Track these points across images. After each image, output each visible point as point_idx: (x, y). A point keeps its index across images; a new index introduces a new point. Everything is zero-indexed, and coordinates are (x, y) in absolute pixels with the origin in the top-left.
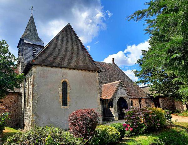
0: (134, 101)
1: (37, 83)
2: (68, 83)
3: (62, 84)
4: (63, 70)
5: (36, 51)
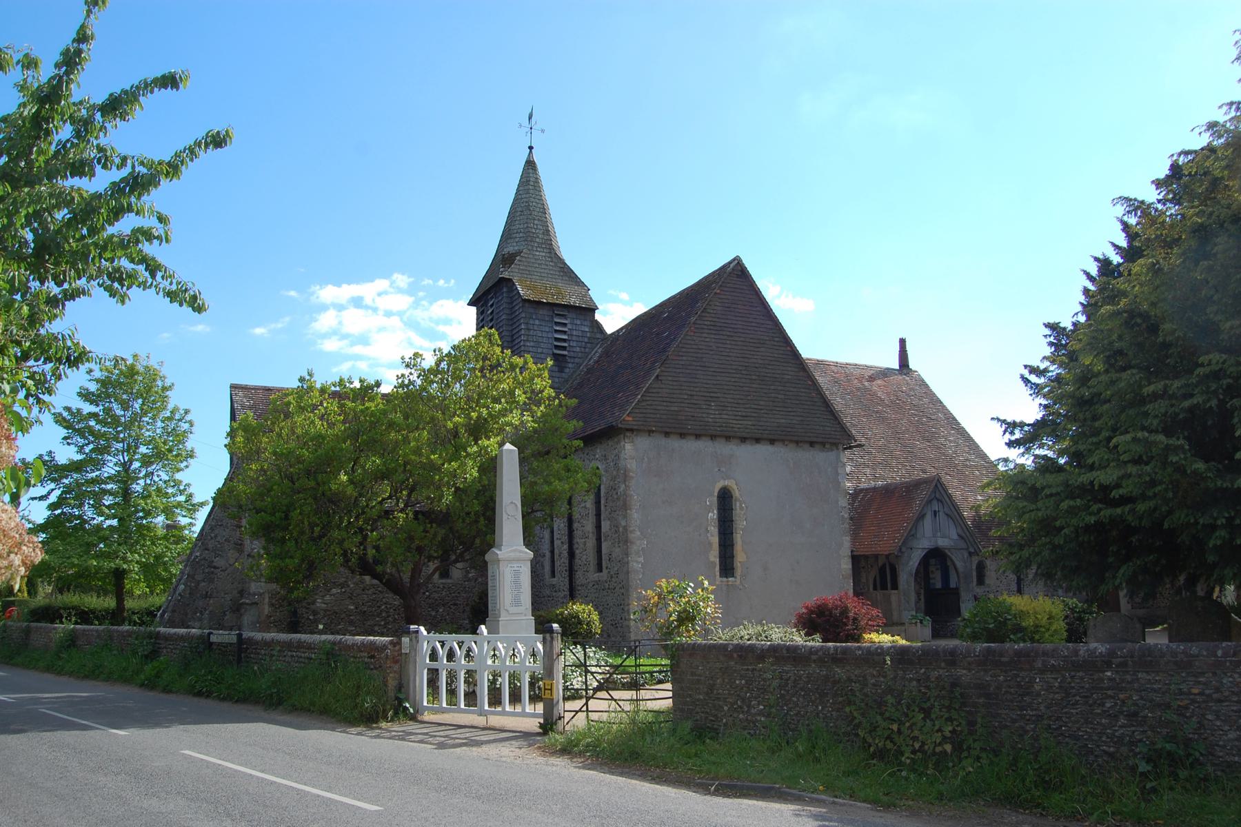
2: (736, 494)
3: (715, 499)
5: (565, 332)
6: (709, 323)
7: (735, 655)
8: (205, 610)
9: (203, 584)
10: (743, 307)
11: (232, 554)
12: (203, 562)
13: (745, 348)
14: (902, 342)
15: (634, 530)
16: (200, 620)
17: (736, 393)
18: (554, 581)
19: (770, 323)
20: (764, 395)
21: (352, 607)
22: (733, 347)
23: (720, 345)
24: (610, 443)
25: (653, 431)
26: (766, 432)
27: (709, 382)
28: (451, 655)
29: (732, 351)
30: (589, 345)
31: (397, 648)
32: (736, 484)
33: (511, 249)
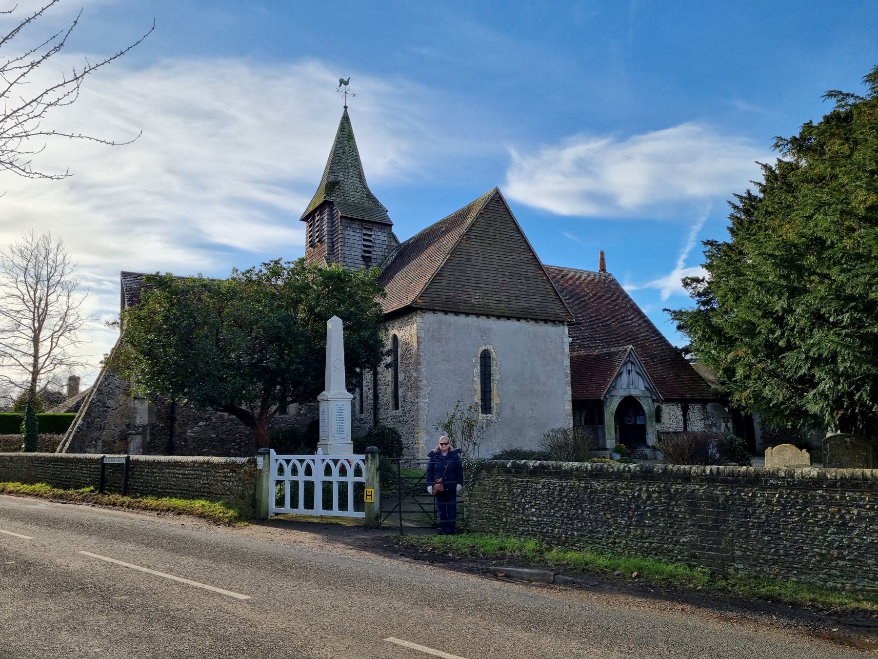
0: (665, 408)
1: (425, 355)
2: (493, 355)
4: (483, 321)
5: (370, 241)
6: (476, 234)
7: (513, 470)
8: (100, 439)
9: (98, 419)
10: (500, 224)
11: (121, 398)
12: (98, 404)
13: (501, 253)
14: (602, 253)
15: (422, 380)
16: (95, 446)
17: (495, 284)
18: (363, 416)
19: (518, 235)
20: (513, 286)
21: (214, 436)
22: (493, 252)
23: (483, 250)
24: (406, 318)
25: (436, 310)
26: (515, 312)
27: (475, 276)
28: (294, 471)
29: (492, 254)
30: (387, 251)
31: (253, 465)
32: (494, 349)
33: (333, 179)
